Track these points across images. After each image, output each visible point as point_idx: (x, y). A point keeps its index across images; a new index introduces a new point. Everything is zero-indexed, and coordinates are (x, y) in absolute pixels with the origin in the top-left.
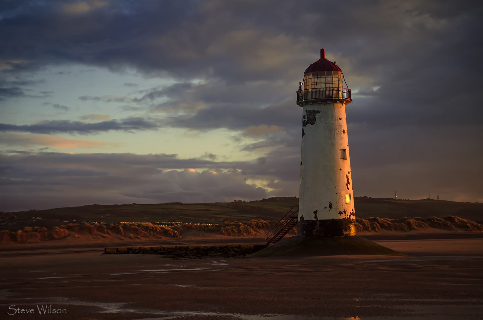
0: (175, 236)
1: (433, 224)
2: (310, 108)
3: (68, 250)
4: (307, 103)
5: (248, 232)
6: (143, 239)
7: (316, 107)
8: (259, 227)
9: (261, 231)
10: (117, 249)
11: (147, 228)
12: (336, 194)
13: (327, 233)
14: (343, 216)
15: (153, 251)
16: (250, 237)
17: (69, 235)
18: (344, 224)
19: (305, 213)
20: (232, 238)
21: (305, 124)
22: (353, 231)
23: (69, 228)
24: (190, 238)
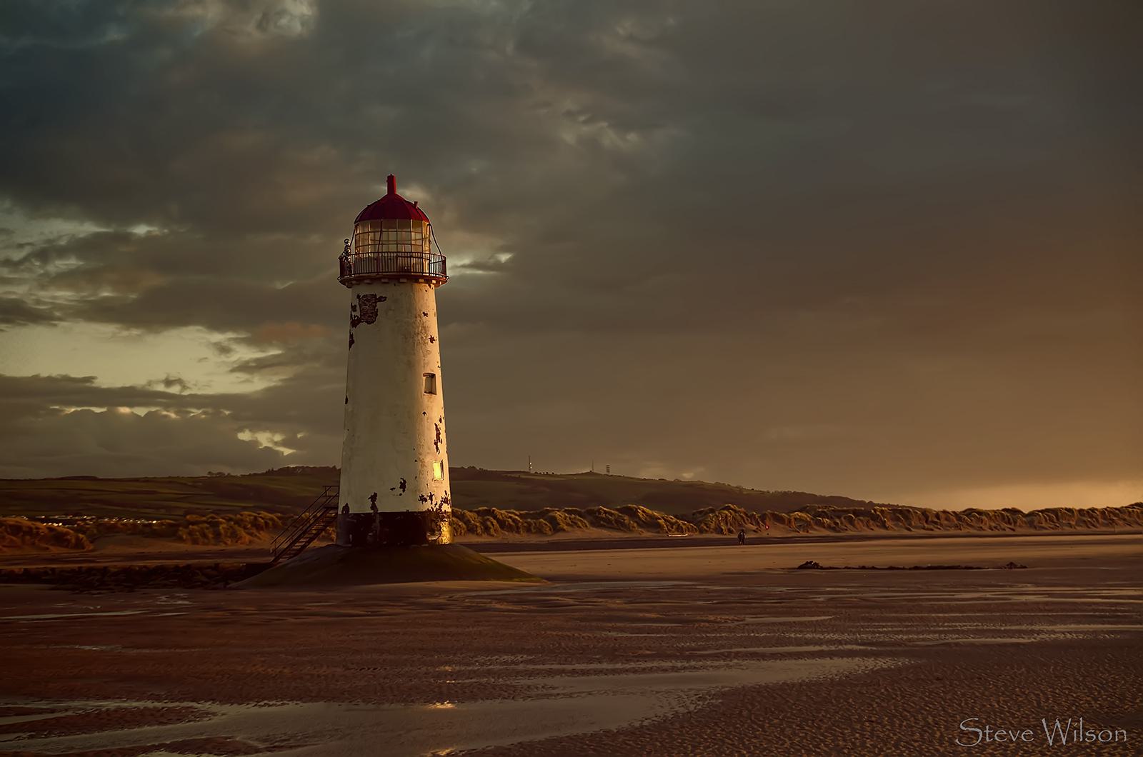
0: (79, 544)
1: (597, 520)
2: (365, 290)
4: (360, 280)
7: (377, 290)
8: (259, 528)
9: (263, 534)
14: (427, 506)
18: (428, 521)
19: (353, 499)
20: (200, 548)
21: (355, 323)
22: (445, 536)
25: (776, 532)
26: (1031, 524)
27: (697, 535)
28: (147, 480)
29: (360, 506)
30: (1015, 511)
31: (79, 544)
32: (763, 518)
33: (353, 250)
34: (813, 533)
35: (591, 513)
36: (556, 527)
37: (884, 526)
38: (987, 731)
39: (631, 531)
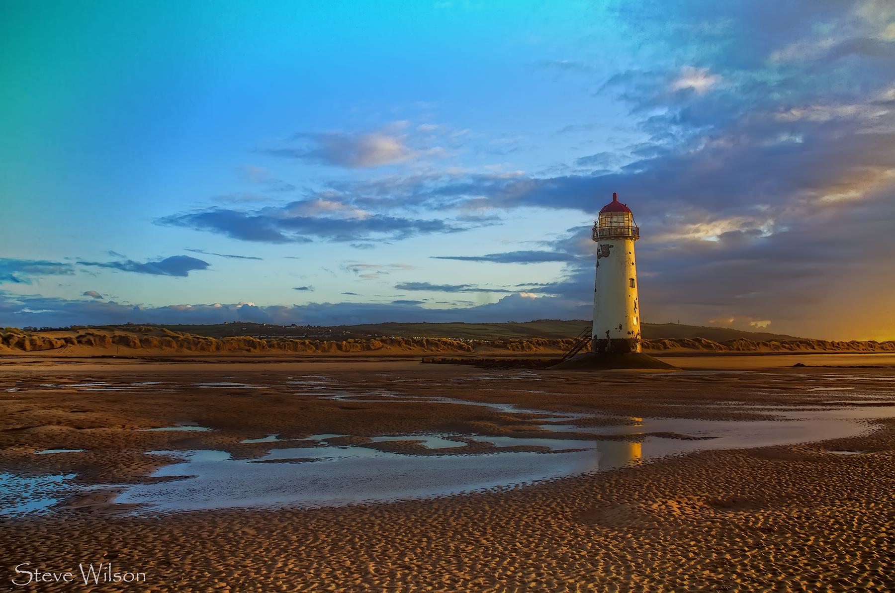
0: (469, 350)
1: (683, 343)
2: (604, 242)
3: (879, 402)
4: (602, 238)
5: (529, 348)
6: (443, 352)
7: (609, 242)
8: (539, 345)
9: (541, 348)
10: (296, 350)
11: (445, 343)
12: (626, 317)
13: (613, 353)
14: (631, 336)
15: (463, 362)
16: (532, 352)
17: (383, 347)
18: (632, 342)
19: (598, 332)
20: (516, 353)
21: (599, 257)
22: (639, 349)
23: (382, 341)
24: (481, 352)
25: (764, 350)
26: (882, 348)
27: (728, 351)
28: (483, 324)
29: (602, 336)
30: (874, 342)
31: (469, 350)
32: (758, 344)
33: (598, 226)
34: (780, 351)
35: (681, 340)
36: (665, 347)
37: (813, 348)
38: (36, 574)
39: (698, 349)
